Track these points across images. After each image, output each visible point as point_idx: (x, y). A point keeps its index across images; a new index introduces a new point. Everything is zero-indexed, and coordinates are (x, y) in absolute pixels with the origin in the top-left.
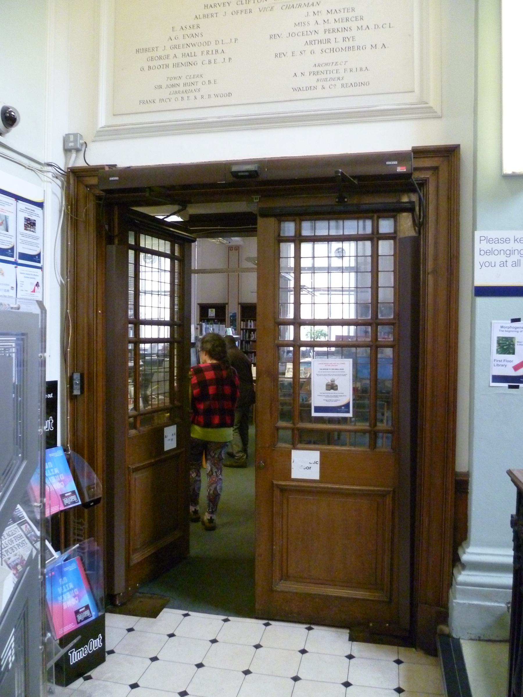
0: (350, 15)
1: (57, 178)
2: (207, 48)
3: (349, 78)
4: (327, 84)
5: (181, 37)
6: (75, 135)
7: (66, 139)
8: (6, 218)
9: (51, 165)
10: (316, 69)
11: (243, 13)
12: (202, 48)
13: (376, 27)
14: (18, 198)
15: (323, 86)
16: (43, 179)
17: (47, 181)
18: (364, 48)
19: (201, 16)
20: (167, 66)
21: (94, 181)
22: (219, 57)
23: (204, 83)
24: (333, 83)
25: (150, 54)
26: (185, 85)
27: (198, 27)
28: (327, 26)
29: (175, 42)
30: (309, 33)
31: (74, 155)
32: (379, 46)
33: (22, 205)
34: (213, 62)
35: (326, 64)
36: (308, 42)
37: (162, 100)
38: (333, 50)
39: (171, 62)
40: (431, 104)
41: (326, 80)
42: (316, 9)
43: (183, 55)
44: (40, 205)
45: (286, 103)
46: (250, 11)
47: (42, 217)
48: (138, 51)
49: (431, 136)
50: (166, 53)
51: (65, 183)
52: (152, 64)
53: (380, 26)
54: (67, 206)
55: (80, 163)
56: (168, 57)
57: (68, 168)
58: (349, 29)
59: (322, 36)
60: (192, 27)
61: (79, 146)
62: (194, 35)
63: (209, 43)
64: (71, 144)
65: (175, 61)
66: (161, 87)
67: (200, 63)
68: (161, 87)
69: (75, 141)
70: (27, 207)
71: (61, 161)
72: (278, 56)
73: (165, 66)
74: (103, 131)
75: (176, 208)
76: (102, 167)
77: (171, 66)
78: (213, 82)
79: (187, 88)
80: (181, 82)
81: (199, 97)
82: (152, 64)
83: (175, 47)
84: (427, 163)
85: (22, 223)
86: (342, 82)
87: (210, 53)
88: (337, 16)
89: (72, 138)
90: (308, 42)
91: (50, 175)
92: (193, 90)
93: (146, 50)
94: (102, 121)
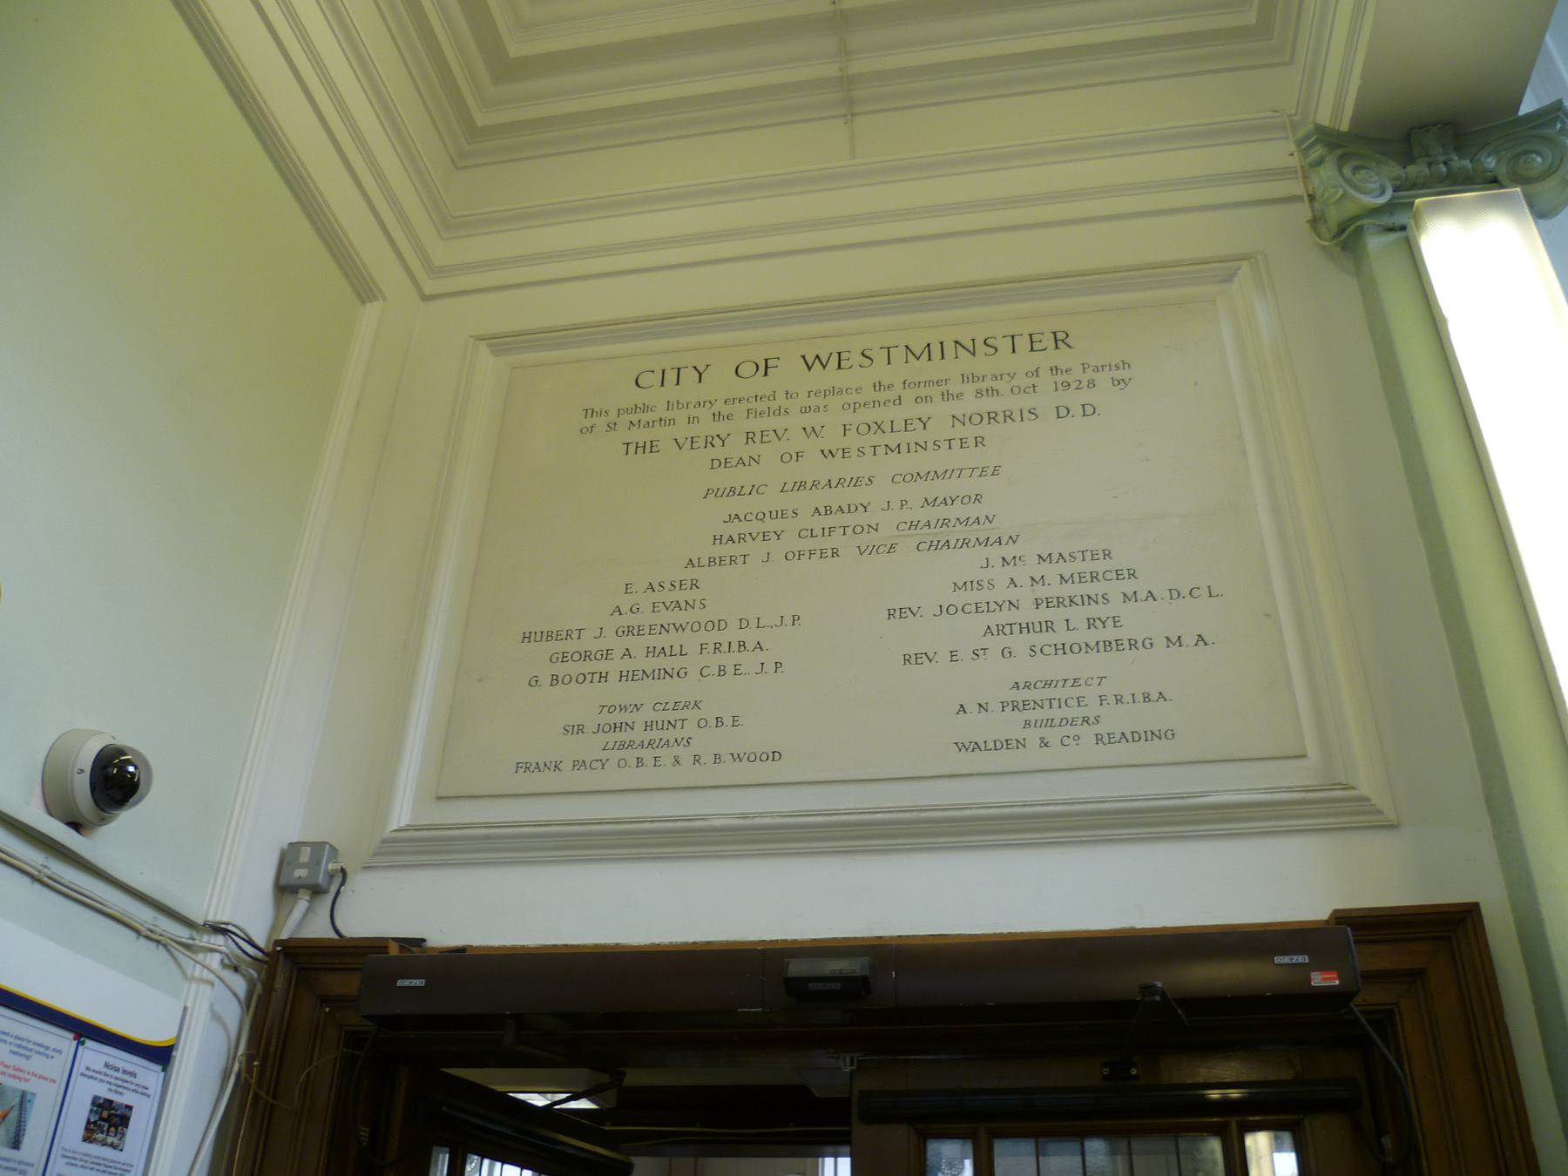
0: (1100, 566)
1: (236, 969)
2: (714, 636)
3: (1116, 719)
4: (1053, 735)
5: (646, 608)
6: (318, 847)
7: (288, 857)
8: (24, 1100)
9: (225, 932)
10: (1021, 695)
11: (815, 557)
12: (704, 636)
13: (1174, 594)
14: (84, 1031)
15: (1042, 739)
16: (189, 973)
17: (201, 980)
18: (1148, 644)
19: (705, 561)
20: (604, 677)
21: (345, 984)
22: (749, 660)
23: (703, 723)
24: (1068, 730)
25: (560, 647)
26: (648, 726)
27: (694, 584)
28: (1041, 592)
29: (628, 620)
30: (993, 606)
31: (302, 905)
32: (1189, 640)
33: (95, 1055)
34: (730, 670)
35: (1048, 684)
36: (994, 630)
37: (579, 764)
38: (1062, 649)
39: (613, 666)
40: (1365, 789)
41: (1050, 723)
42: (1009, 551)
43: (651, 652)
44: (161, 1055)
45: (939, 782)
46: (835, 553)
47: (157, 1099)
48: (527, 637)
49: (1376, 876)
50: (603, 644)
51: (259, 988)
52: (560, 669)
53: (1185, 592)
54: (250, 1058)
55: (318, 929)
56: (607, 654)
57: (277, 942)
58: (1101, 600)
59: (1027, 614)
60: (677, 585)
61: (321, 879)
62: (683, 605)
63: (723, 625)
64: (301, 873)
65: (628, 665)
66: (580, 729)
67: (694, 673)
68: (580, 729)
69: (315, 862)
70: (112, 1061)
71: (257, 920)
72: (913, 660)
73: (597, 677)
74: (395, 840)
75: (583, 1075)
76: (376, 946)
77: (614, 677)
78: (728, 721)
79: (655, 734)
80: (639, 718)
81: (687, 760)
82: (560, 669)
83: (630, 631)
84: (1383, 958)
85: (79, 1112)
86: (1097, 729)
87: (725, 648)
88: (1067, 569)
89: (305, 855)
90: (994, 630)
91: (214, 961)
92: (672, 741)
93: (550, 636)
94: (401, 814)
